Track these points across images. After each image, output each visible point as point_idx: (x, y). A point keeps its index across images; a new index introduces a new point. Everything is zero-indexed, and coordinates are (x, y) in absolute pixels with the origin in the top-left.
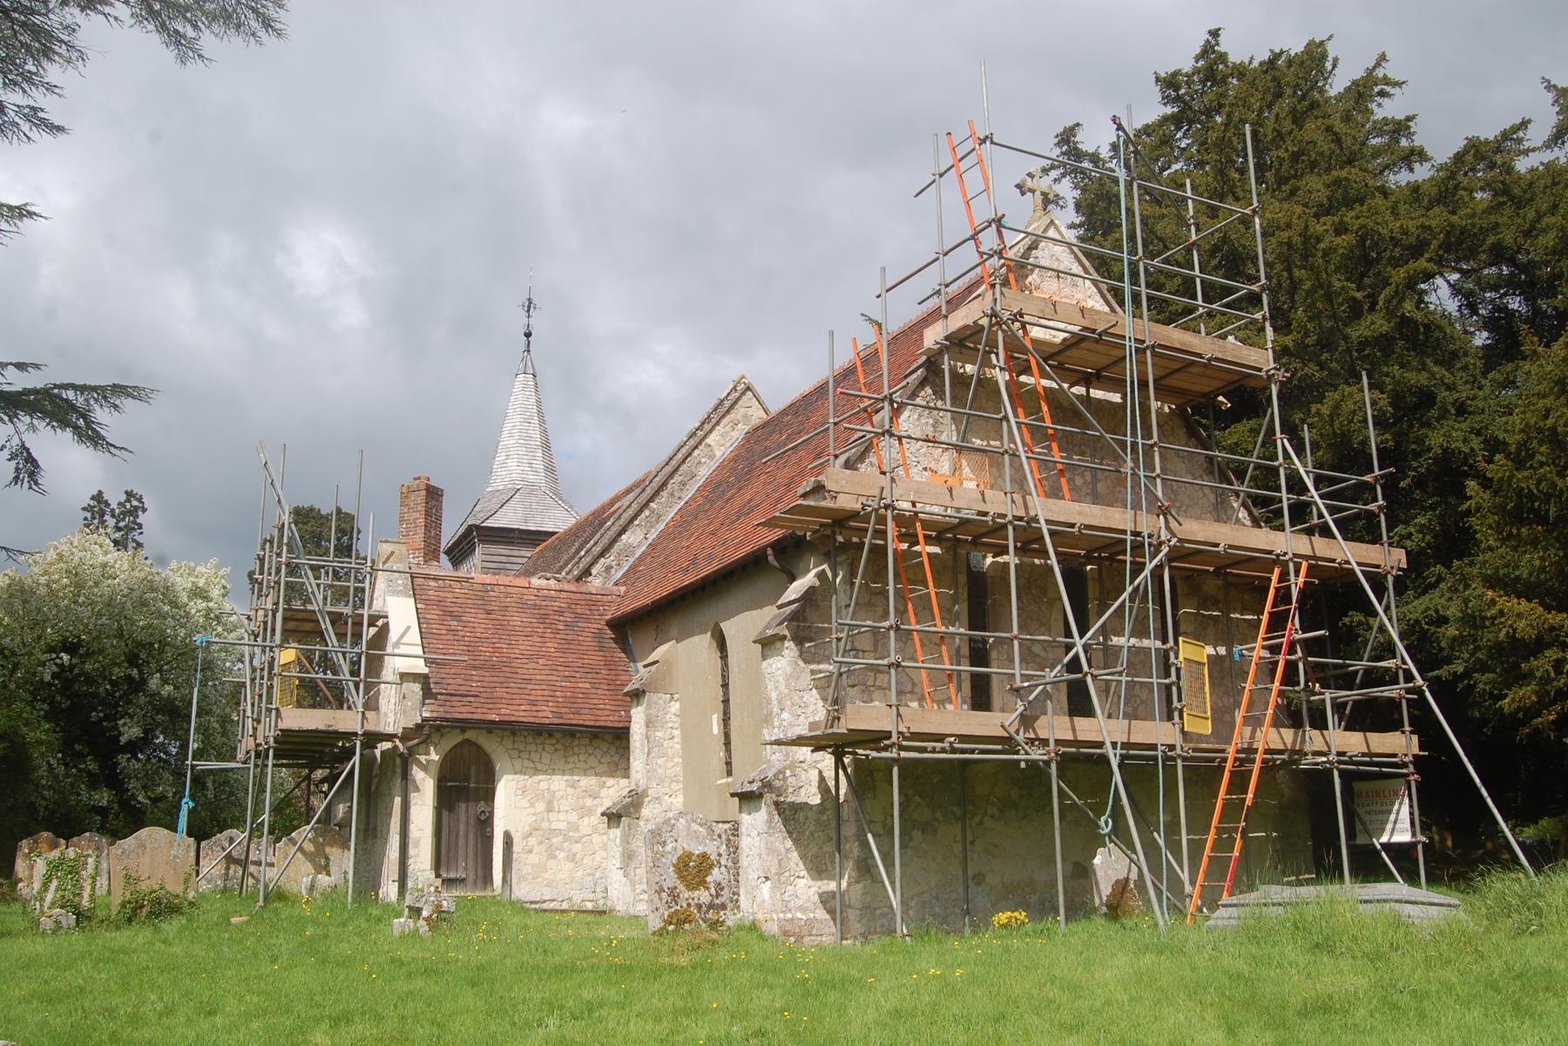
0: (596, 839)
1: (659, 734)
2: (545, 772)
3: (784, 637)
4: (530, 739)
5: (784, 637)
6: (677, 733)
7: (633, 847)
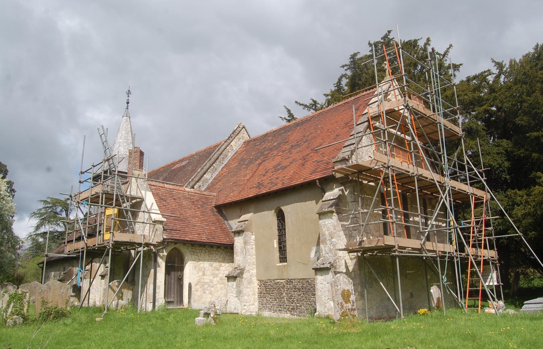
0: (219, 286)
1: (248, 247)
2: (202, 261)
3: (333, 212)
4: (197, 248)
5: (333, 212)
6: (254, 246)
7: (241, 289)
